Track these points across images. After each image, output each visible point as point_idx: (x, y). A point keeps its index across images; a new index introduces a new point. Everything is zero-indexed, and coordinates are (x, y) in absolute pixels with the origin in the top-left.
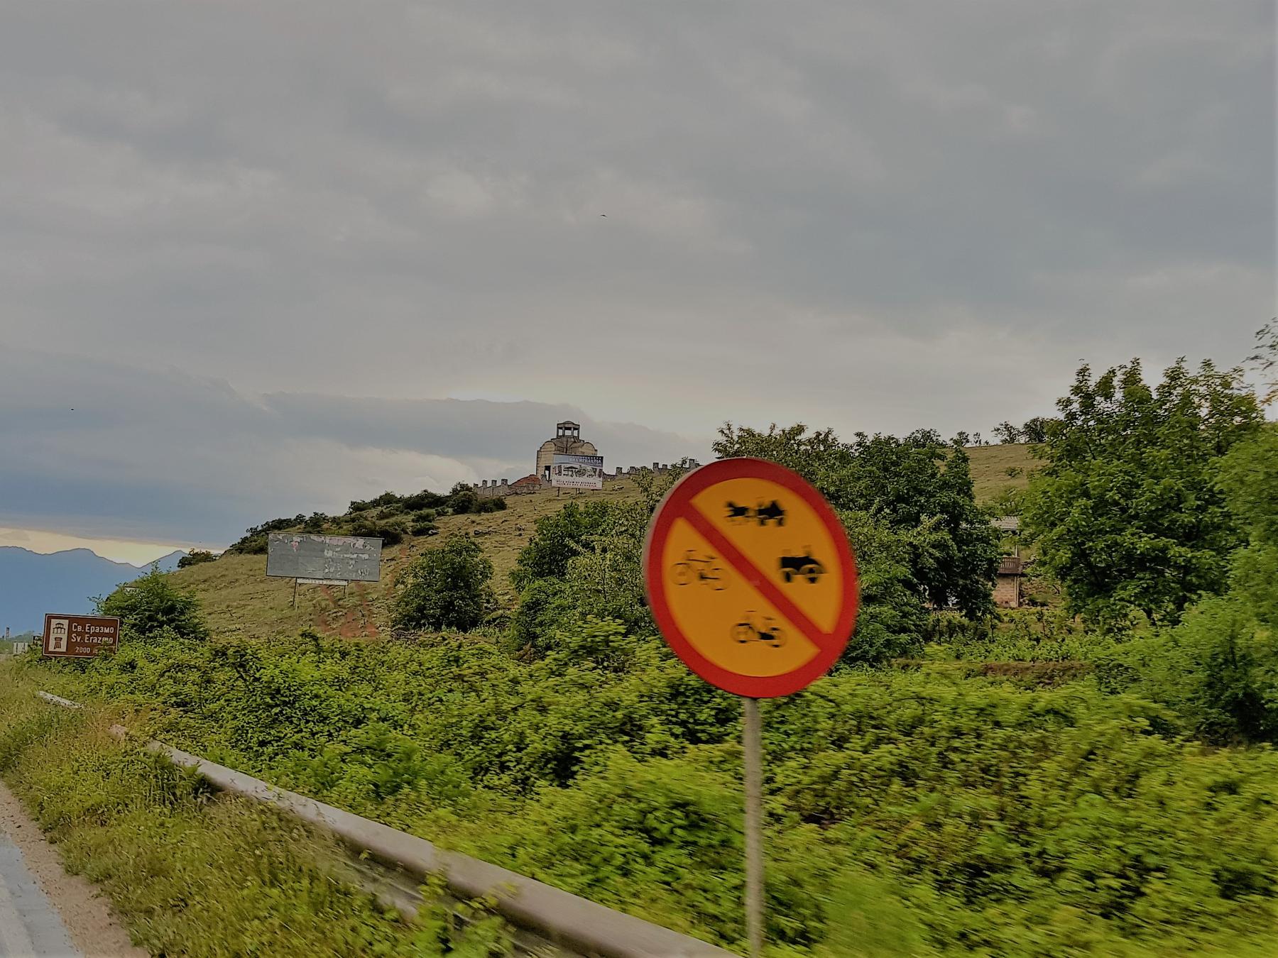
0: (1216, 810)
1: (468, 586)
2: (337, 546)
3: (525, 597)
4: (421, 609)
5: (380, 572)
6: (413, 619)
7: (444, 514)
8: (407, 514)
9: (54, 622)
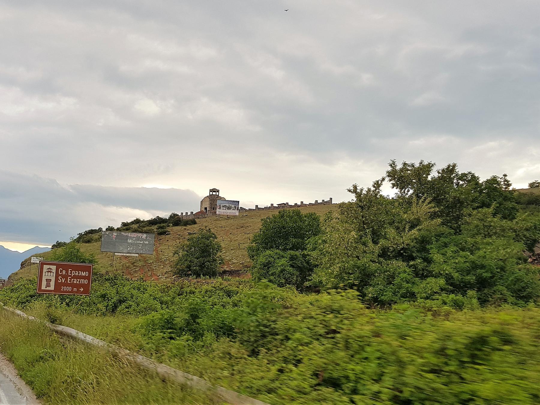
0: (339, 333)
2: (134, 237)
4: (189, 267)
5: (170, 249)
6: (183, 272)
7: (168, 226)
8: (151, 226)
9: (46, 267)
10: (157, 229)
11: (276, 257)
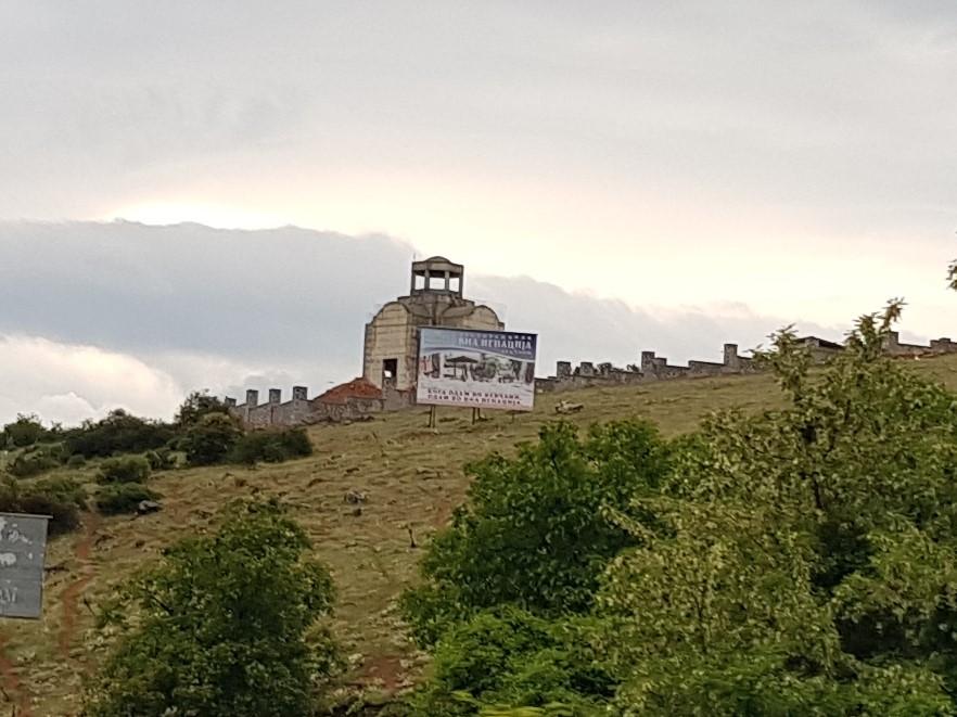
1: (274, 629)
3: (450, 651)
4: (166, 684)
7: (167, 465)
8: (78, 464)
10: (99, 480)
11: (511, 643)
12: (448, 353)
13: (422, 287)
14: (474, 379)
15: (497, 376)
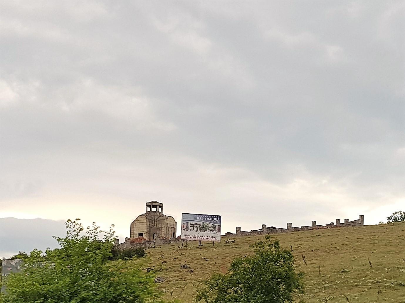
12: (191, 222)
13: (149, 211)
14: (200, 231)
15: (208, 230)
